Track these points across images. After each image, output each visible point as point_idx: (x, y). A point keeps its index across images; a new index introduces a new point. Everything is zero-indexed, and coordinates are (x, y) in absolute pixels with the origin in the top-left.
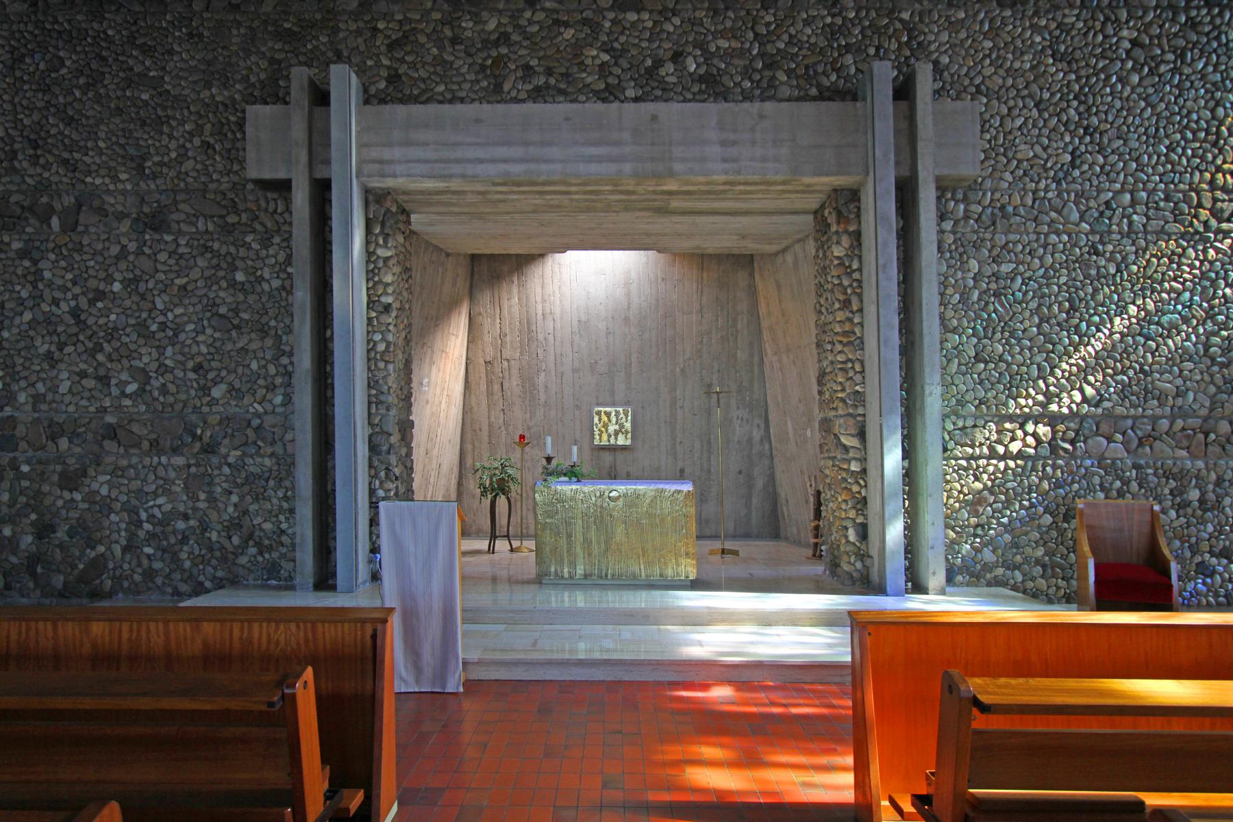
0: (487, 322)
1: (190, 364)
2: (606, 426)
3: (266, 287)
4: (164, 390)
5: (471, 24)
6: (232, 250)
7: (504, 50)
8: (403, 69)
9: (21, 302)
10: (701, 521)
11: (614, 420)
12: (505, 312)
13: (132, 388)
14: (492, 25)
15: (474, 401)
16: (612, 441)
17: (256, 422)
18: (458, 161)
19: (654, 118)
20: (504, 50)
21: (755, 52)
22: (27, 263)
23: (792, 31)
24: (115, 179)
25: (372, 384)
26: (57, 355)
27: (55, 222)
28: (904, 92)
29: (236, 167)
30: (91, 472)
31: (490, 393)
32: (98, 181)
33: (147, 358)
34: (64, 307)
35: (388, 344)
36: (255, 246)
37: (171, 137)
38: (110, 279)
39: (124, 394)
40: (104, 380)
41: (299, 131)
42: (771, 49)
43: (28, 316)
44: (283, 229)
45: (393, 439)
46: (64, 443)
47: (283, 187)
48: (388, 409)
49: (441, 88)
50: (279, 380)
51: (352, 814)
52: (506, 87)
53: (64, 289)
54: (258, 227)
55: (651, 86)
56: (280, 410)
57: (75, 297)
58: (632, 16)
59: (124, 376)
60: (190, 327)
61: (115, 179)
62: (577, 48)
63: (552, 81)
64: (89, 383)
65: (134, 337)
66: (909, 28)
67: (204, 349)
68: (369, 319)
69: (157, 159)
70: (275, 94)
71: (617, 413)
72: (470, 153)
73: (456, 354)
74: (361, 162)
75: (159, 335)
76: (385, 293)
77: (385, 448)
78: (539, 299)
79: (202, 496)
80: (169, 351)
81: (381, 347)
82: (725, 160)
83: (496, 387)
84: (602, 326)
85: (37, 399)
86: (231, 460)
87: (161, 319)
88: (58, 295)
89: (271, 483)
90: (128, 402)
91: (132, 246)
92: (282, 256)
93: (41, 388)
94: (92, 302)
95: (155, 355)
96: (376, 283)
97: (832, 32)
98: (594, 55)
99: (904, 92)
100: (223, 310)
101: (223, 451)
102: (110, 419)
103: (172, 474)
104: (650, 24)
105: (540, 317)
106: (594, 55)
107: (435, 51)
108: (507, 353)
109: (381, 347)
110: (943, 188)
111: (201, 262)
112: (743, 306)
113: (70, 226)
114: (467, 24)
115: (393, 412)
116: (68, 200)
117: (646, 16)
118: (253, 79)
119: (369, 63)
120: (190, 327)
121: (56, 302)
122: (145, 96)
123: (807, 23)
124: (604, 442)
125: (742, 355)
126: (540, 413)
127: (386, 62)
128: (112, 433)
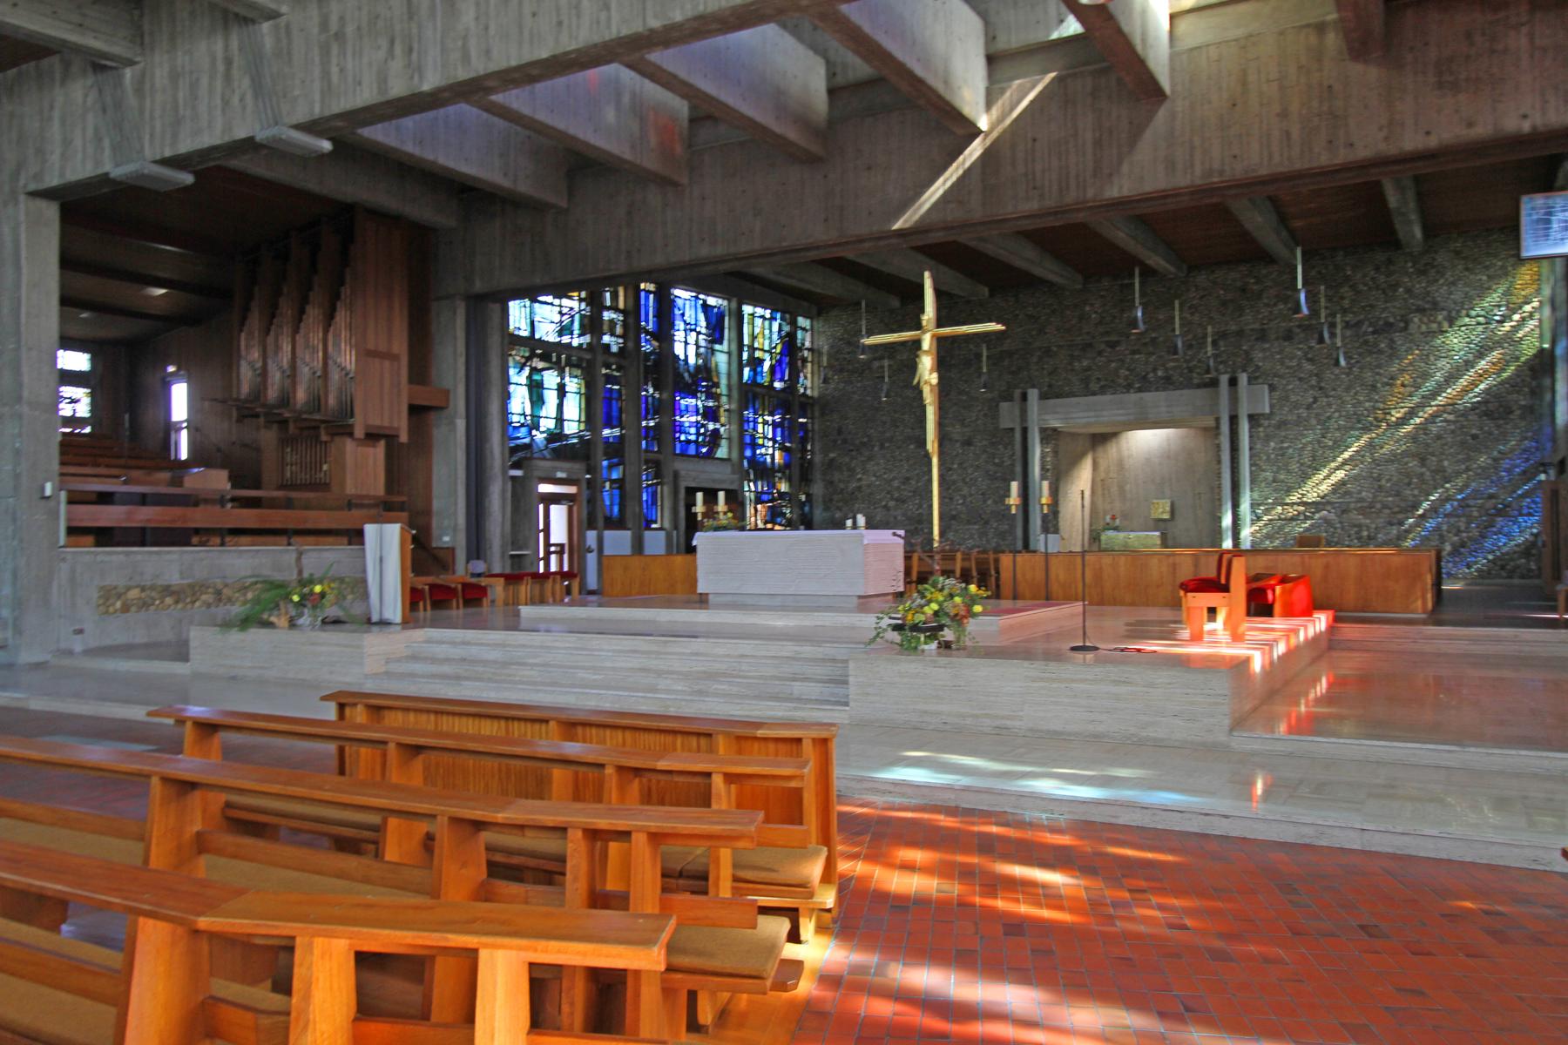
10: (66, 910)
28: (1233, 382)
33: (965, 491)
41: (1017, 412)
44: (1011, 443)
47: (1012, 430)
51: (360, 131)
55: (1145, 385)
66: (1247, 353)
70: (1009, 398)
106: (1124, 372)
110: (1251, 417)
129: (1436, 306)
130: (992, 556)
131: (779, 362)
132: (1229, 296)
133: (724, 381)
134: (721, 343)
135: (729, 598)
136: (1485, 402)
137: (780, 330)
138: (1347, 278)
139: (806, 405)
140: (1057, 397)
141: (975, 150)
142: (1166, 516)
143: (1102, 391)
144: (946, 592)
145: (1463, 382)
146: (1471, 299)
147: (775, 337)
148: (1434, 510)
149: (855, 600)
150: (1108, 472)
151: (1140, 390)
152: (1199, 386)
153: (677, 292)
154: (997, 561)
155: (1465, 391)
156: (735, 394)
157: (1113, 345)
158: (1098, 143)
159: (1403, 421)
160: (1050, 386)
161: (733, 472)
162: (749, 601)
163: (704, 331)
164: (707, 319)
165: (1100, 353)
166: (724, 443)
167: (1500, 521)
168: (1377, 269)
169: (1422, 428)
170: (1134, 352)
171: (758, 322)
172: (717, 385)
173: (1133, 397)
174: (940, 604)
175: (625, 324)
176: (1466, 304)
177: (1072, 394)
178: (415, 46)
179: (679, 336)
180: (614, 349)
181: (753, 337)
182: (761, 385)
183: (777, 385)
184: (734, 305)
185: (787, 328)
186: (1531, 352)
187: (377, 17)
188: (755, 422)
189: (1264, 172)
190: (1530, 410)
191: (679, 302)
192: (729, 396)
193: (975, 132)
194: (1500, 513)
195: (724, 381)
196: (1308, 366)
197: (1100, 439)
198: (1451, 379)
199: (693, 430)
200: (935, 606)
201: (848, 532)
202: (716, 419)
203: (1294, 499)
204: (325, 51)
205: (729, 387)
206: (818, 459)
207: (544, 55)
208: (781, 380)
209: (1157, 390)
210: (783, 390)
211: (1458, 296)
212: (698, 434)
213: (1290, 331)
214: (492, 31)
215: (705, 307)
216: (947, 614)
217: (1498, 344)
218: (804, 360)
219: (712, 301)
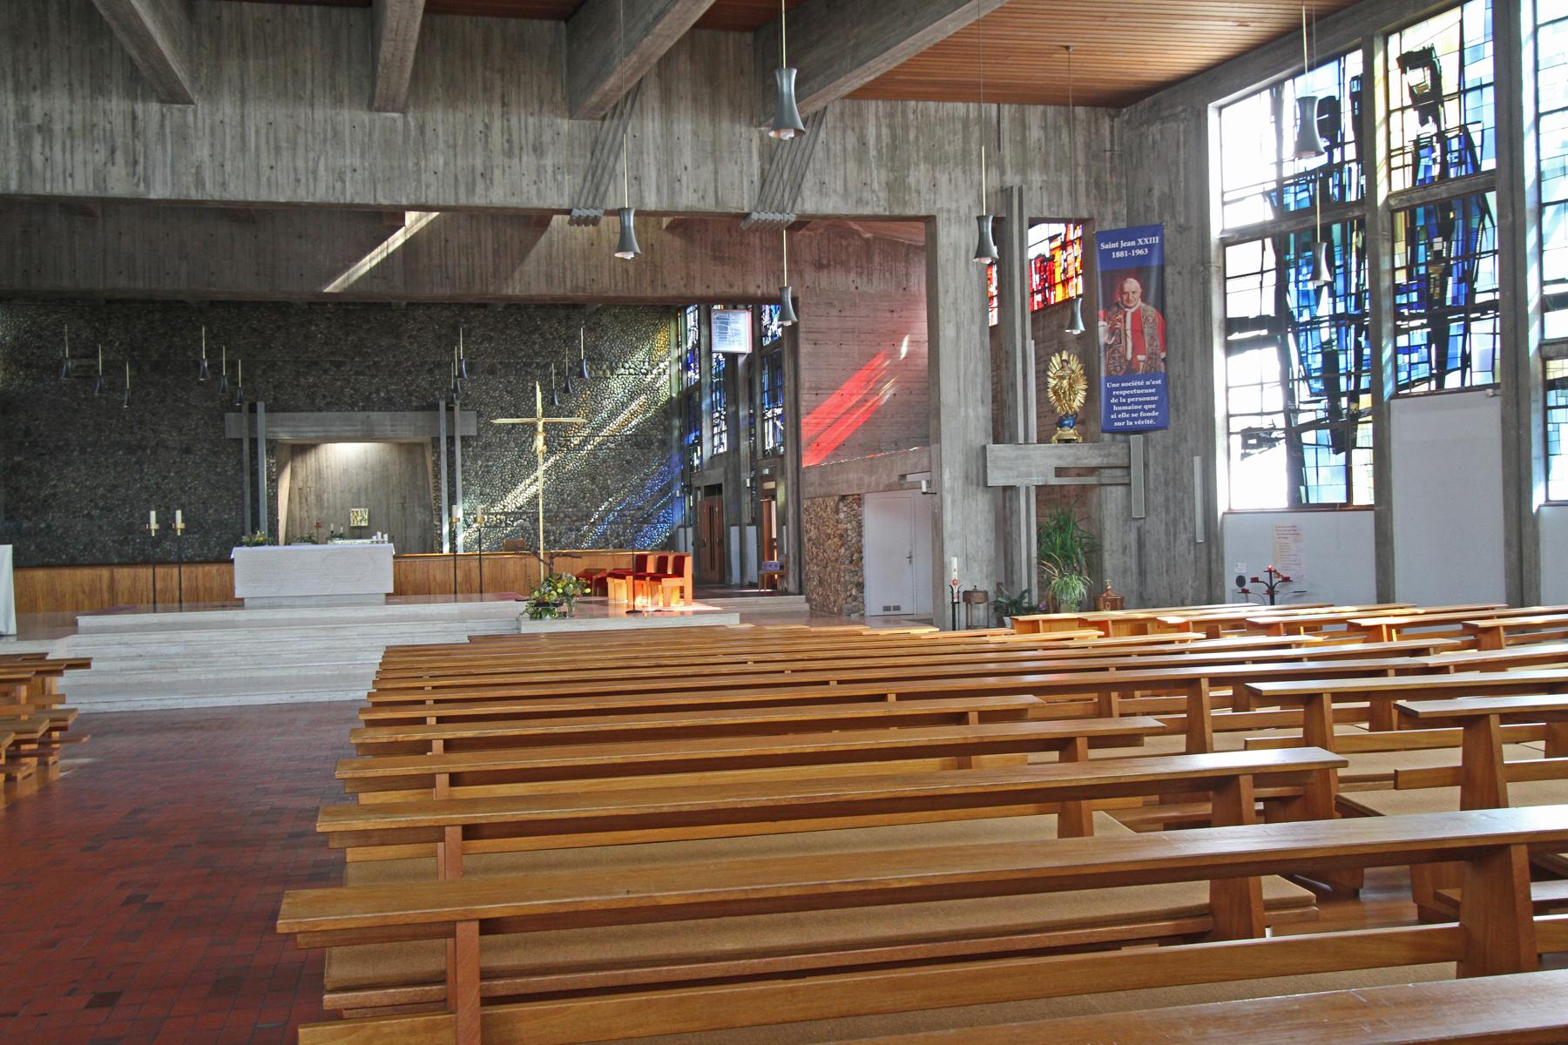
0: (299, 470)
28: (450, 409)
41: (245, 423)
47: (239, 441)
62: (342, 388)
97: (432, 383)
99: (450, 409)
110: (463, 438)
112: (419, 461)
113: (154, 452)
116: (153, 443)
125: (420, 483)
129: (601, 357)
132: (443, 331)
135: (266, 601)
136: (635, 435)
138: (537, 328)
140: (284, 410)
142: (364, 524)
143: (329, 407)
145: (621, 418)
146: (625, 354)
148: (602, 519)
151: (364, 409)
152: (417, 409)
155: (622, 426)
157: (338, 365)
158: (496, 252)
159: (580, 446)
160: (275, 399)
162: (285, 602)
165: (325, 371)
167: (646, 527)
168: (560, 322)
169: (593, 453)
170: (357, 373)
176: (623, 357)
177: (297, 409)
178: (141, 160)
186: (664, 399)
187: (94, 125)
189: (611, 294)
190: (663, 443)
194: (645, 521)
196: (508, 398)
197: (301, 449)
198: (613, 415)
203: (498, 509)
204: (25, 139)
207: (282, 200)
211: (616, 351)
213: (493, 365)
214: (228, 167)
217: (643, 391)
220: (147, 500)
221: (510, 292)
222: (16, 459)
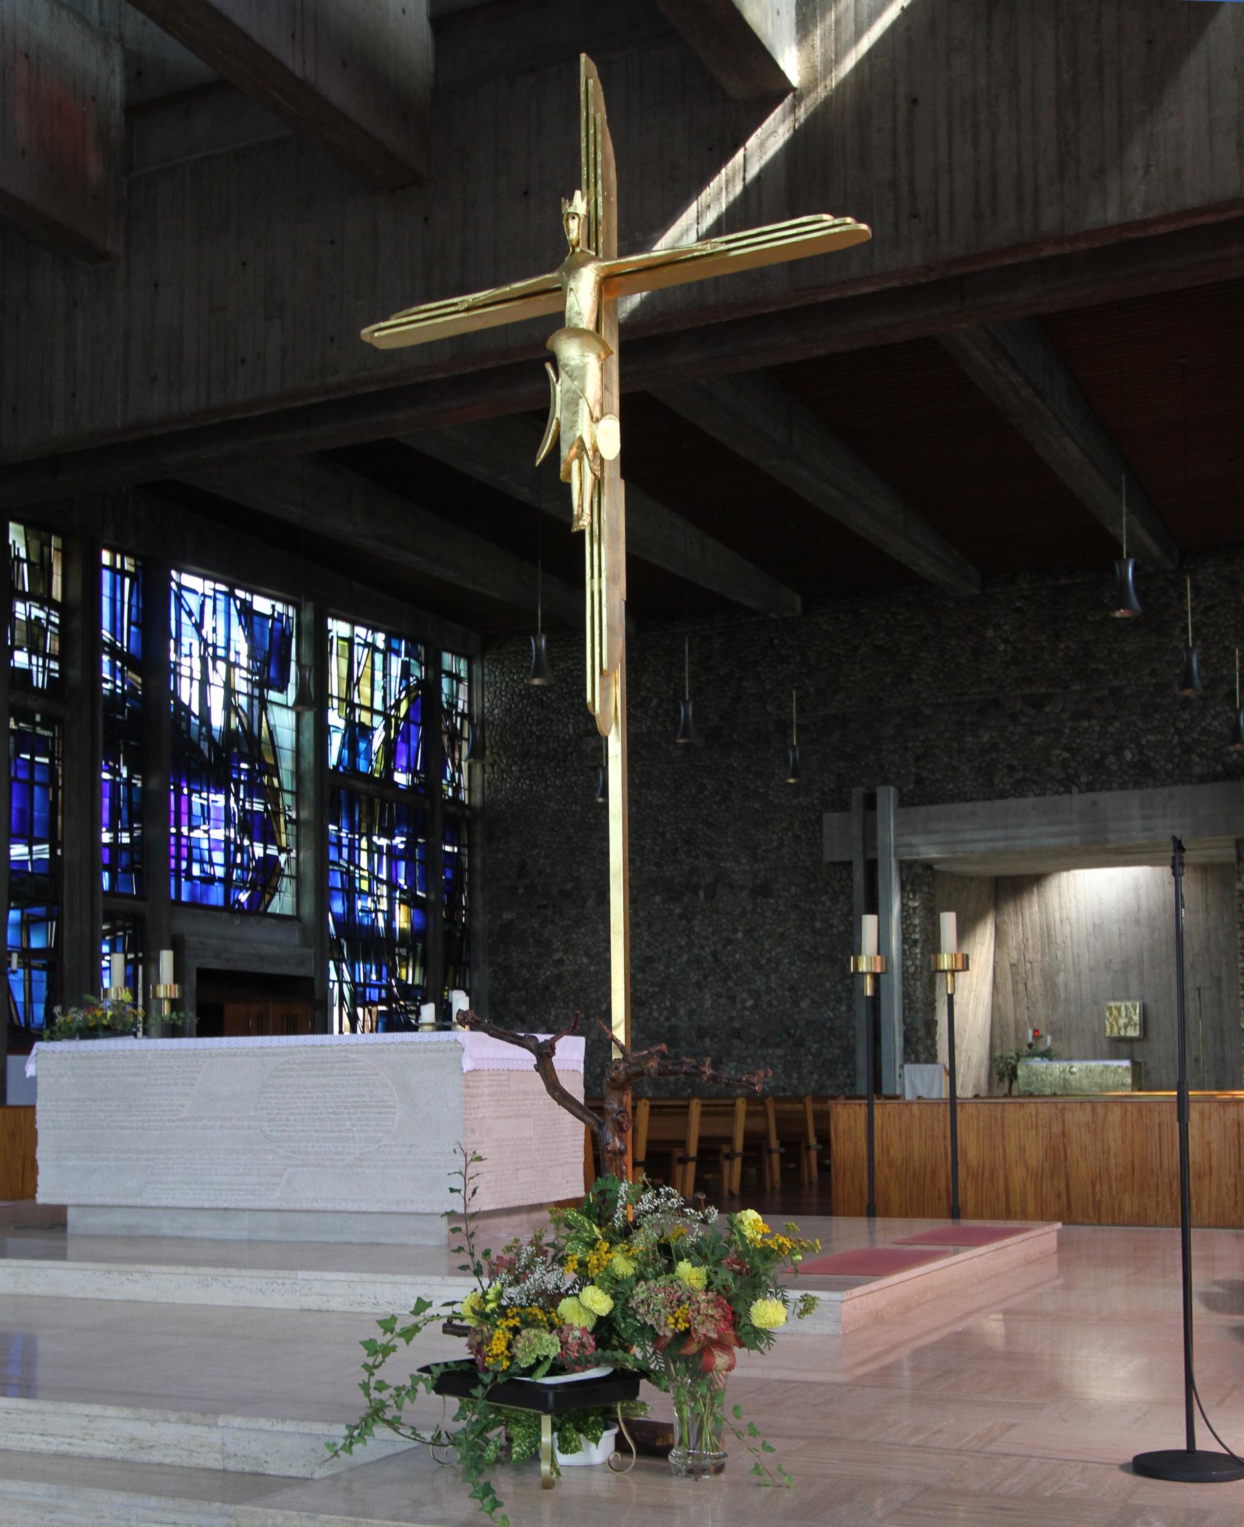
0: (1011, 929)
1: (787, 986)
2: (1116, 1020)
3: (835, 931)
4: (770, 1004)
5: (971, 739)
6: (813, 906)
7: (994, 755)
8: (925, 774)
9: (681, 948)
11: (1124, 1014)
12: (1027, 920)
13: (749, 1003)
14: (986, 738)
15: (1001, 999)
16: (1122, 1033)
17: (829, 1025)
18: (960, 842)
19: (1095, 803)
20: (994, 755)
21: (1175, 742)
22: (684, 922)
23: (1203, 724)
24: (737, 862)
25: (906, 995)
26: (703, 983)
27: (701, 893)
29: (815, 850)
30: (725, 1061)
31: (1015, 992)
32: (728, 865)
33: (759, 983)
34: (707, 950)
35: (916, 967)
36: (828, 903)
37: (773, 832)
38: (735, 931)
39: (745, 1008)
40: (732, 999)
41: (857, 830)
42: (1187, 739)
43: (685, 957)
45: (920, 1034)
46: (707, 1041)
47: (847, 865)
48: (917, 1012)
49: (951, 786)
50: (844, 995)
52: (996, 781)
53: (707, 938)
54: (830, 890)
56: (845, 1015)
57: (714, 944)
58: (1085, 724)
59: (745, 996)
60: (786, 961)
61: (737, 862)
63: (1028, 775)
64: (723, 1001)
65: (751, 969)
67: (795, 975)
68: (904, 951)
69: (764, 848)
70: (842, 805)
71: (1126, 1007)
72: (968, 836)
73: (983, 959)
74: (896, 847)
75: (767, 967)
76: (914, 932)
77: (914, 1040)
78: (1056, 906)
79: (795, 1075)
80: (773, 977)
81: (912, 970)
82: (1145, 830)
83: (1021, 987)
84: (1115, 928)
85: (692, 1012)
86: (813, 1050)
87: (768, 956)
88: (703, 942)
89: (840, 1066)
90: (747, 1013)
91: (749, 907)
92: (845, 909)
93: (693, 1005)
94: (724, 947)
95: (764, 980)
96: (908, 926)
98: (1058, 754)
100: (807, 948)
101: (808, 1044)
102: (736, 1025)
103: (775, 1061)
104: (1097, 728)
105: (1058, 923)
106: (1058, 754)
107: (946, 760)
108: (1030, 955)
109: (912, 970)
111: (793, 916)
114: (969, 739)
115: (920, 1015)
116: (710, 879)
117: (1094, 722)
118: (826, 789)
119: (903, 772)
120: (786, 961)
121: (702, 947)
122: (757, 806)
123: (1214, 717)
124: (1115, 1034)
126: (1061, 1009)
127: (913, 770)
128: (737, 1034)
130: (810, 1107)
131: (405, 736)
133: (287, 764)
134: (282, 688)
137: (406, 672)
139: (457, 820)
141: (770, 138)
142: (1133, 1032)
143: (1019, 789)
144: (642, 1241)
147: (395, 685)
149: (443, 1225)
150: (1023, 947)
151: (1090, 787)
152: (1202, 779)
153: (188, 580)
154: (823, 1118)
156: (309, 788)
160: (919, 781)
161: (305, 942)
162: (169, 1227)
163: (244, 661)
164: (250, 638)
166: (286, 885)
170: (1077, 716)
171: (360, 653)
172: (274, 771)
173: (1078, 800)
174: (618, 1289)
175: (64, 631)
177: (960, 797)
179: (190, 666)
180: (39, 680)
181: (351, 682)
182: (368, 777)
183: (401, 778)
184: (308, 616)
185: (417, 672)
188: (353, 848)
191: (192, 601)
192: (297, 794)
193: (770, 88)
195: (287, 764)
197: (1008, 888)
199: (218, 857)
200: (598, 1301)
201: (426, 1036)
202: (269, 837)
205: (298, 774)
206: (481, 923)
208: (407, 770)
209: (1123, 786)
210: (411, 789)
212: (229, 864)
215: (247, 612)
216: (647, 1331)
218: (455, 736)
219: (262, 605)
220: (698, 985)
221: (1112, 215)
222: (507, 916)
